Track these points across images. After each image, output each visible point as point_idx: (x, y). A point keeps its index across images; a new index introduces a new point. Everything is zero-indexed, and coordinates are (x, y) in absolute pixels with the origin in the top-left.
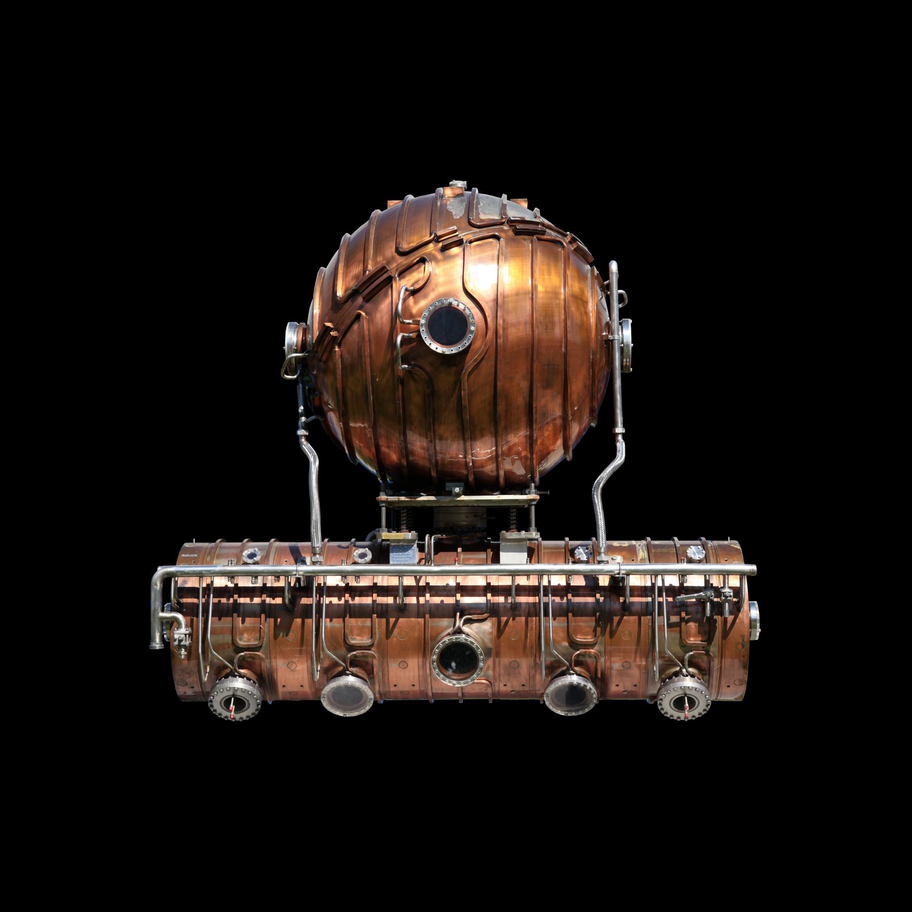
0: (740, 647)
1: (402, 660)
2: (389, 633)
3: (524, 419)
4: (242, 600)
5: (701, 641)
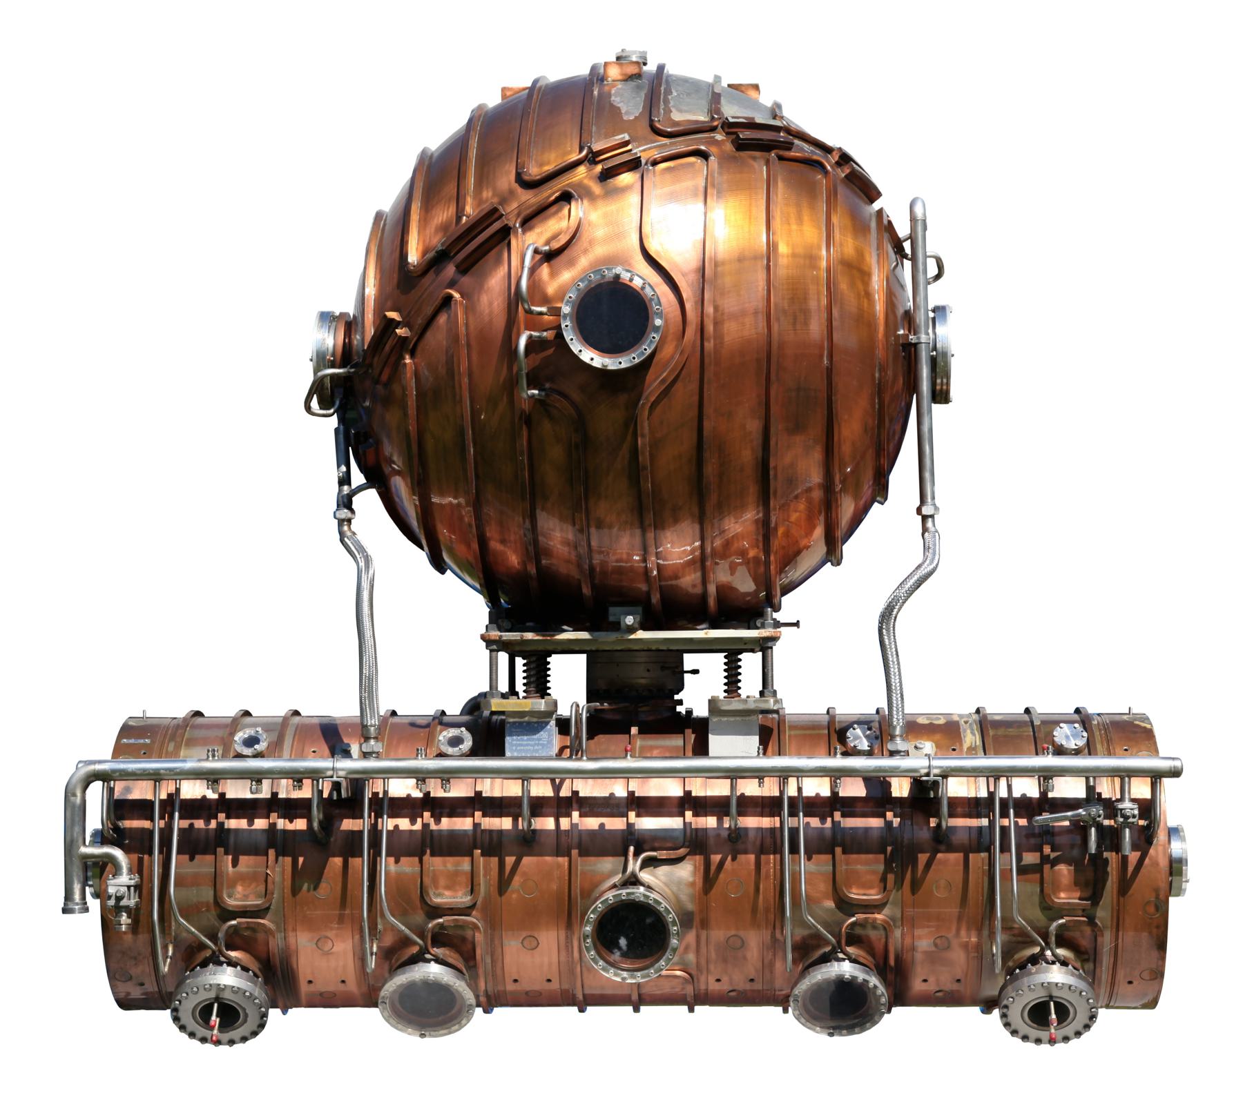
2: (503, 883)
3: (753, 490)
4: (233, 824)
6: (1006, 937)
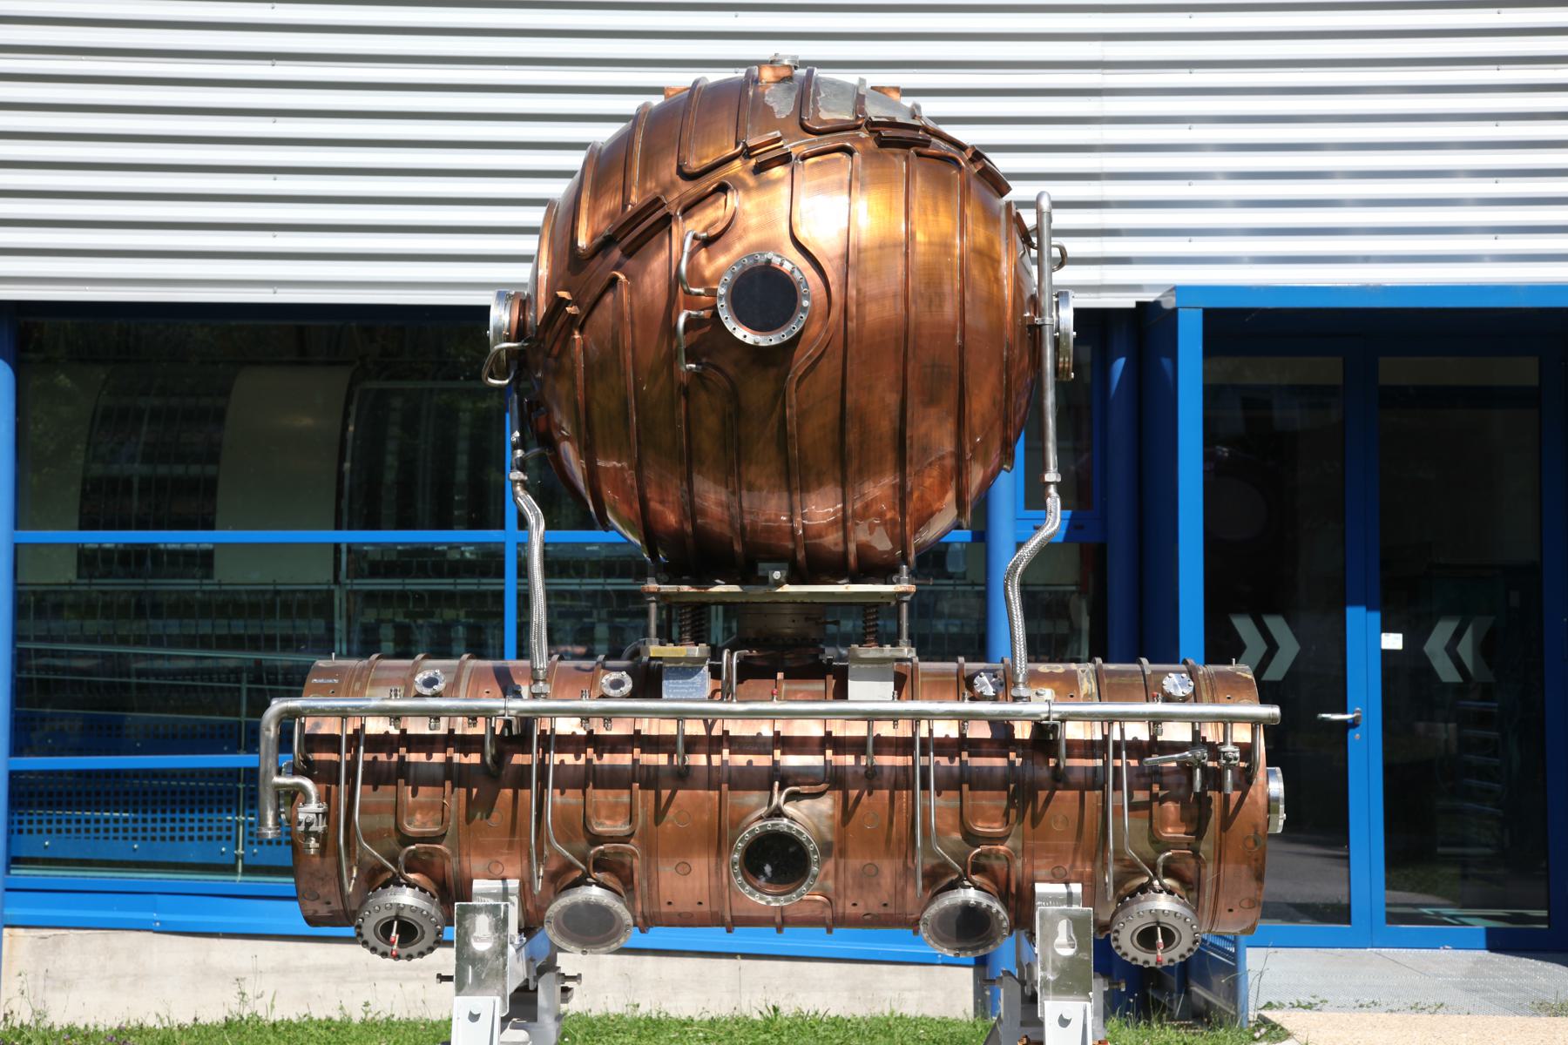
0: (1250, 844)
1: (682, 860)
2: (659, 814)
3: (890, 457)
4: (413, 757)
6: (1117, 868)
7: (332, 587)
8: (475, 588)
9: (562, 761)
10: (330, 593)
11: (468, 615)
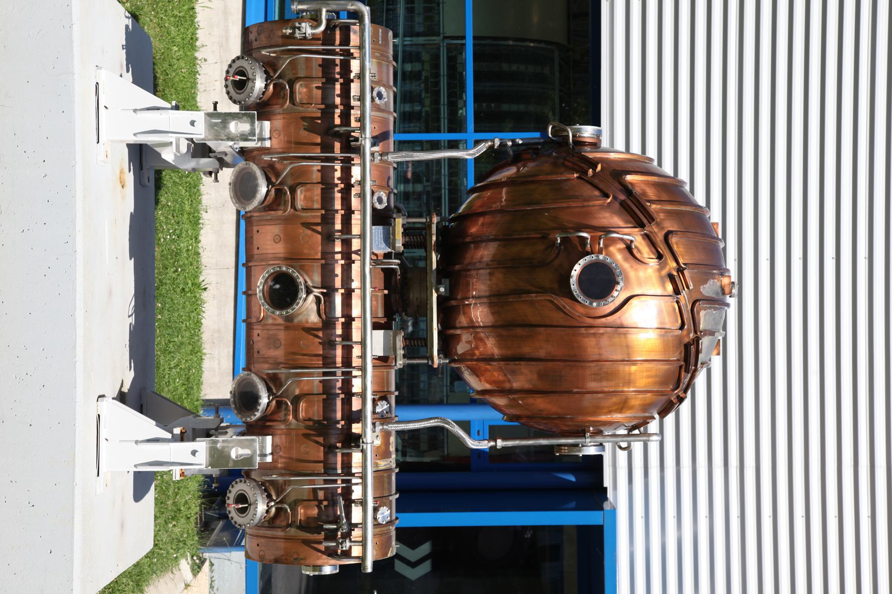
0: (295, 556)
2: (308, 225)
4: (338, 86)
5: (300, 520)
7: (442, 36)
8: (442, 116)
9: (336, 170)
10: (438, 34)
11: (427, 112)
